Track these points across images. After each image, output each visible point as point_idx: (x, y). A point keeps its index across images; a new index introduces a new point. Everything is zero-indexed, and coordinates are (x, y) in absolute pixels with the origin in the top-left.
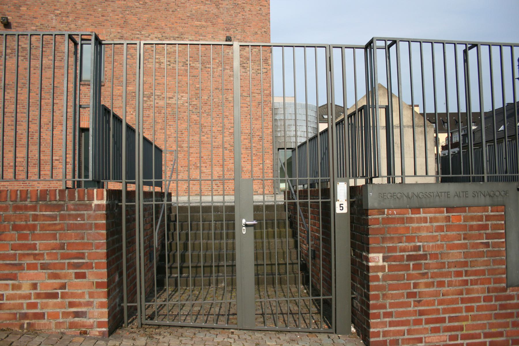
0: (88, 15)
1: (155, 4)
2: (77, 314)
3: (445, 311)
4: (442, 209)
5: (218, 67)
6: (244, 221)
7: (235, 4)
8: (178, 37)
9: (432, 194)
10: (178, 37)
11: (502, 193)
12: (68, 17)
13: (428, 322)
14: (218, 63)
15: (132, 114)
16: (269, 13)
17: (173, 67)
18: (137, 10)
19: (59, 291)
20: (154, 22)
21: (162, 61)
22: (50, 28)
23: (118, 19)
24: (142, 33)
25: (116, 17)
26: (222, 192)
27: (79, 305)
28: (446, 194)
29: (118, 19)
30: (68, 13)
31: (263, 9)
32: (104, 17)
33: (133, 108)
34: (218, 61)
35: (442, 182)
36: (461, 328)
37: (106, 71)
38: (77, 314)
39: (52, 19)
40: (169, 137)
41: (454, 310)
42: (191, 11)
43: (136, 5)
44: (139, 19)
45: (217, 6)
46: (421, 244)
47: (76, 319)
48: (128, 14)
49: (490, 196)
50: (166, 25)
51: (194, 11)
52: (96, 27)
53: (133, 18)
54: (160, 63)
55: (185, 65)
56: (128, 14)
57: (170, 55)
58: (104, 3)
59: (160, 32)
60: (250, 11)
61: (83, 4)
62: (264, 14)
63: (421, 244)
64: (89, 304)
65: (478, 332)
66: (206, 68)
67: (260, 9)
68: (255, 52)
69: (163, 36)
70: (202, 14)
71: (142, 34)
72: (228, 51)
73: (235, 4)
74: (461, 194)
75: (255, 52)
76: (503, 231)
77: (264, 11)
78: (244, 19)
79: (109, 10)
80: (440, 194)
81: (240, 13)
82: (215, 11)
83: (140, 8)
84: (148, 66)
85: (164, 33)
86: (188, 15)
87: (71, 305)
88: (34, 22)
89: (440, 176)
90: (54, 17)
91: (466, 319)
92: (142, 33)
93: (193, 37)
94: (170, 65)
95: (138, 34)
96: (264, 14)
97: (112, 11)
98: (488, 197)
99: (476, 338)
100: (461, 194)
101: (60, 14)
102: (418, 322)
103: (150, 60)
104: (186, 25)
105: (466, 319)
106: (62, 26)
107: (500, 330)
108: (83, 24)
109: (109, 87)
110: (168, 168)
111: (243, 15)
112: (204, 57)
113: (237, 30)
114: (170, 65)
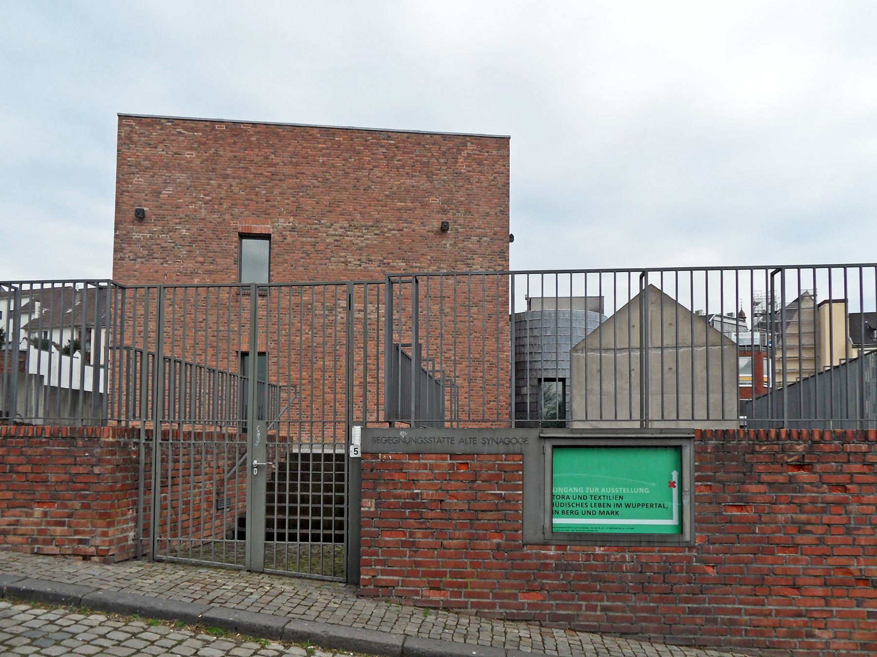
0: (247, 200)
1: (339, 181)
2: (81, 542)
3: (446, 565)
4: (444, 456)
5: (429, 266)
6: (255, 462)
7: (457, 173)
8: (371, 226)
9: (433, 440)
10: (371, 226)
11: (520, 441)
12: (221, 204)
13: (425, 574)
14: (430, 260)
15: (307, 333)
16: (509, 184)
17: (365, 268)
18: (315, 190)
19: (66, 520)
20: (338, 207)
21: (349, 260)
22: (197, 220)
23: (288, 204)
24: (322, 221)
25: (286, 201)
26: (332, 439)
27: (83, 533)
28: (450, 440)
29: (288, 204)
30: (222, 198)
31: (498, 178)
32: (269, 203)
33: (309, 325)
34: (429, 257)
35: (516, 427)
36: (465, 585)
37: (273, 276)
38: (81, 542)
39: (201, 209)
40: (358, 364)
41: (456, 565)
42: (391, 188)
43: (313, 184)
44: (318, 203)
45: (430, 177)
46: (419, 491)
47: (81, 546)
48: (302, 197)
49: (504, 443)
50: (355, 210)
51: (395, 188)
52: (258, 216)
53: (310, 201)
54: (346, 263)
55: (382, 265)
56: (302, 197)
57: (361, 252)
58: (270, 182)
59: (347, 220)
60: (478, 182)
61: (241, 186)
62: (500, 185)
63: (419, 491)
64: (91, 532)
65: (486, 591)
66: (412, 267)
67: (494, 178)
68: (485, 242)
69: (350, 226)
70: (408, 192)
71: (322, 224)
72: (444, 242)
73: (457, 173)
74: (468, 440)
75: (485, 242)
76: (521, 482)
77: (501, 180)
78: (469, 194)
79: (276, 191)
80: (442, 440)
81: (462, 187)
82: (427, 185)
83: (318, 187)
84: (330, 267)
85: (353, 220)
86: (387, 193)
87: (77, 533)
88: (177, 213)
89: (514, 421)
90: (203, 206)
91: (471, 575)
92: (322, 221)
93: (394, 225)
94: (360, 265)
95: (316, 224)
96: (500, 185)
97: (280, 193)
98: (501, 444)
99: (483, 598)
100: (468, 440)
101: (211, 201)
102: (415, 574)
103: (332, 259)
104: (384, 208)
105: (471, 575)
106: (213, 216)
107: (514, 591)
108: (242, 213)
109: (275, 297)
110: (357, 406)
111: (467, 189)
112: (410, 252)
113: (459, 212)
114: (360, 265)
